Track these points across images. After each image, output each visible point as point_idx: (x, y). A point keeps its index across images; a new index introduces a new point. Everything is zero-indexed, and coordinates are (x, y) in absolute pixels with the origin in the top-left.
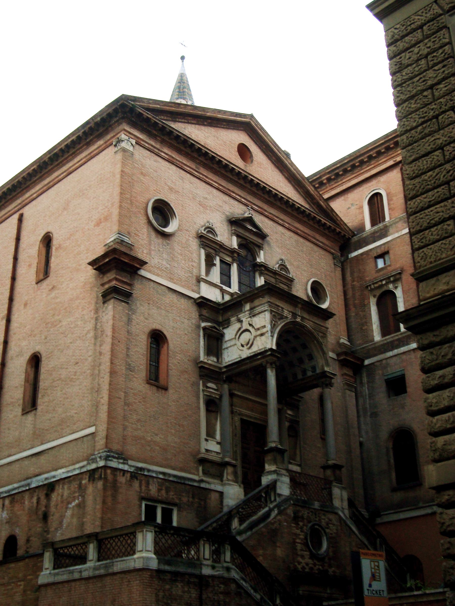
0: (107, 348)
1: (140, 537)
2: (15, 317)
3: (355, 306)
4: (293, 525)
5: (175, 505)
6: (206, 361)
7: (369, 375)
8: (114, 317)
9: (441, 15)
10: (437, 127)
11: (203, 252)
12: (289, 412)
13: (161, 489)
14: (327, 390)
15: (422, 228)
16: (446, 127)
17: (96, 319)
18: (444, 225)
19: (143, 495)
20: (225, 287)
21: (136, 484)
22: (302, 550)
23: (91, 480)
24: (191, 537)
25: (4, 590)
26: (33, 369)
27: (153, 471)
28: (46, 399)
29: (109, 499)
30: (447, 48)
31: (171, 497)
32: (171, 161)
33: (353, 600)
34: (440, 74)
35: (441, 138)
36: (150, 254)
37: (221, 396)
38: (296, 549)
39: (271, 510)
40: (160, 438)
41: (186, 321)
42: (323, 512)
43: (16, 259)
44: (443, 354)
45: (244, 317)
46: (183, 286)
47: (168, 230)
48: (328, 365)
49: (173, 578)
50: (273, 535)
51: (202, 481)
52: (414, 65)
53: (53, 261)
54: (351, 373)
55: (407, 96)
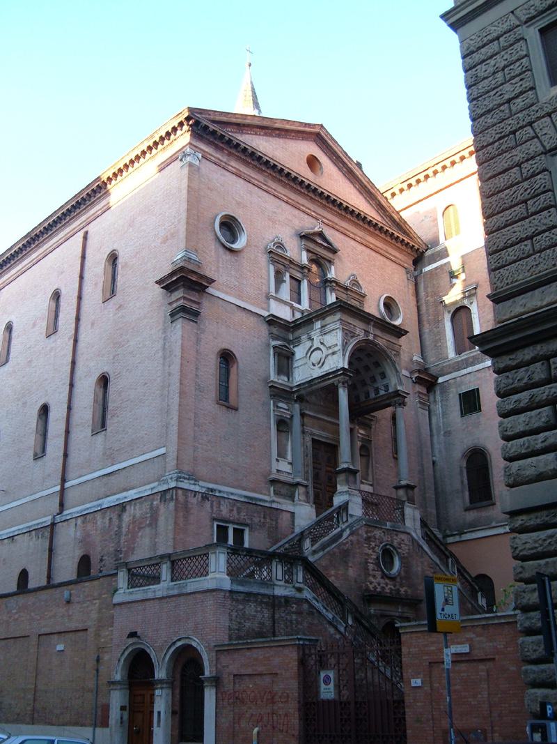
0: (176, 368)
1: (212, 557)
2: (81, 337)
3: (429, 322)
4: (365, 545)
5: (247, 525)
6: (276, 380)
7: (442, 393)
8: (182, 336)
9: (518, 26)
10: (514, 143)
11: (272, 268)
12: (361, 431)
13: (232, 510)
14: (399, 410)
15: (499, 248)
16: (523, 143)
17: (165, 339)
18: (521, 246)
19: (214, 515)
20: (295, 305)
21: (208, 504)
22: (373, 570)
23: (163, 501)
24: (265, 558)
25: (80, 608)
26: (102, 389)
27: (224, 492)
28: (116, 420)
29: (181, 521)
30: (524, 60)
31: (242, 517)
32: (238, 175)
33: (426, 622)
34: (517, 88)
35: (518, 154)
36: (218, 271)
37: (292, 416)
38: (368, 569)
39: (343, 531)
40: (231, 459)
41: (256, 340)
42: (395, 533)
43: (81, 277)
44: (518, 378)
45: (315, 335)
46: (253, 304)
47: (234, 246)
48: (401, 383)
49: (247, 599)
50: (345, 554)
51: (273, 501)
52: (491, 78)
53: (120, 279)
54: (424, 391)
55: (483, 111)
